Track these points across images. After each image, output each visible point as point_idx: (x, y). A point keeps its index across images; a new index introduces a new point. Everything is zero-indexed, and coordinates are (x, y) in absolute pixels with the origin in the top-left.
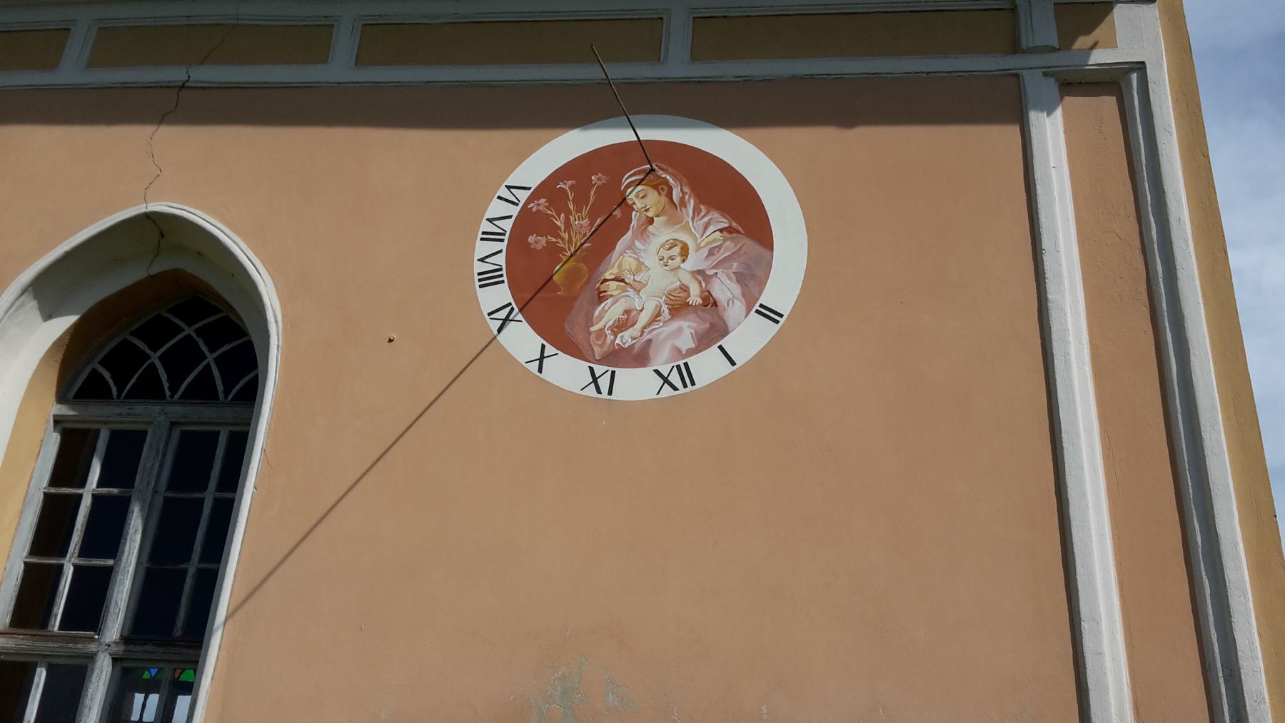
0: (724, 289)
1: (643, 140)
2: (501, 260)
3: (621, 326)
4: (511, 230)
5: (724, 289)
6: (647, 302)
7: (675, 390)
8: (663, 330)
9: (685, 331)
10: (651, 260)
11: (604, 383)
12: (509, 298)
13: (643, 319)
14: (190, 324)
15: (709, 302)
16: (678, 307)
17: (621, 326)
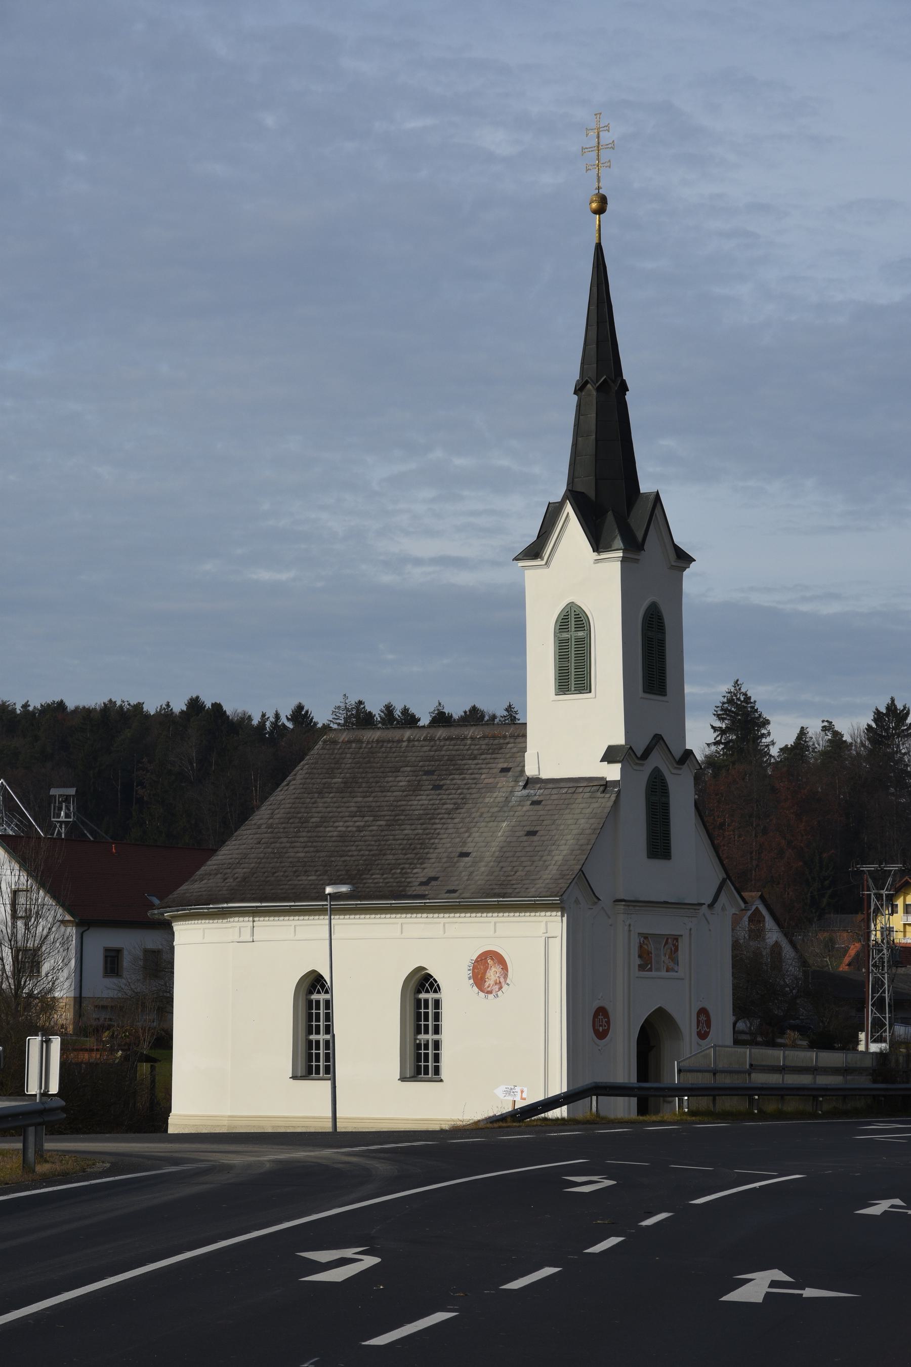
0: (502, 980)
1: (292, 1075)
2: (471, 974)
3: (488, 987)
4: (555, 1267)
5: (502, 980)
6: (492, 982)
7: (772, 1281)
8: (494, 987)
9: (497, 987)
10: (492, 974)
11: (487, 997)
12: (473, 982)
13: (491, 985)
14: (426, 985)
15: (500, 982)
16: (496, 984)
17: (488, 987)
